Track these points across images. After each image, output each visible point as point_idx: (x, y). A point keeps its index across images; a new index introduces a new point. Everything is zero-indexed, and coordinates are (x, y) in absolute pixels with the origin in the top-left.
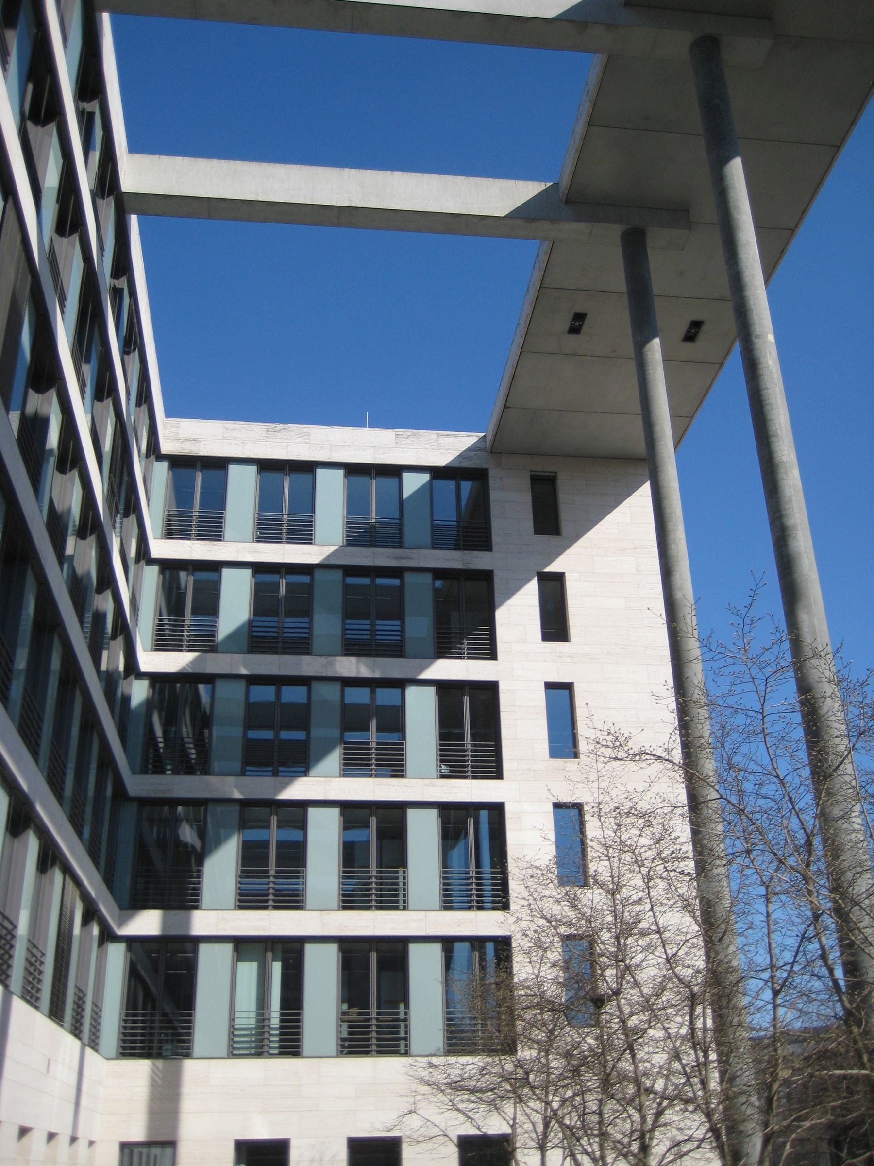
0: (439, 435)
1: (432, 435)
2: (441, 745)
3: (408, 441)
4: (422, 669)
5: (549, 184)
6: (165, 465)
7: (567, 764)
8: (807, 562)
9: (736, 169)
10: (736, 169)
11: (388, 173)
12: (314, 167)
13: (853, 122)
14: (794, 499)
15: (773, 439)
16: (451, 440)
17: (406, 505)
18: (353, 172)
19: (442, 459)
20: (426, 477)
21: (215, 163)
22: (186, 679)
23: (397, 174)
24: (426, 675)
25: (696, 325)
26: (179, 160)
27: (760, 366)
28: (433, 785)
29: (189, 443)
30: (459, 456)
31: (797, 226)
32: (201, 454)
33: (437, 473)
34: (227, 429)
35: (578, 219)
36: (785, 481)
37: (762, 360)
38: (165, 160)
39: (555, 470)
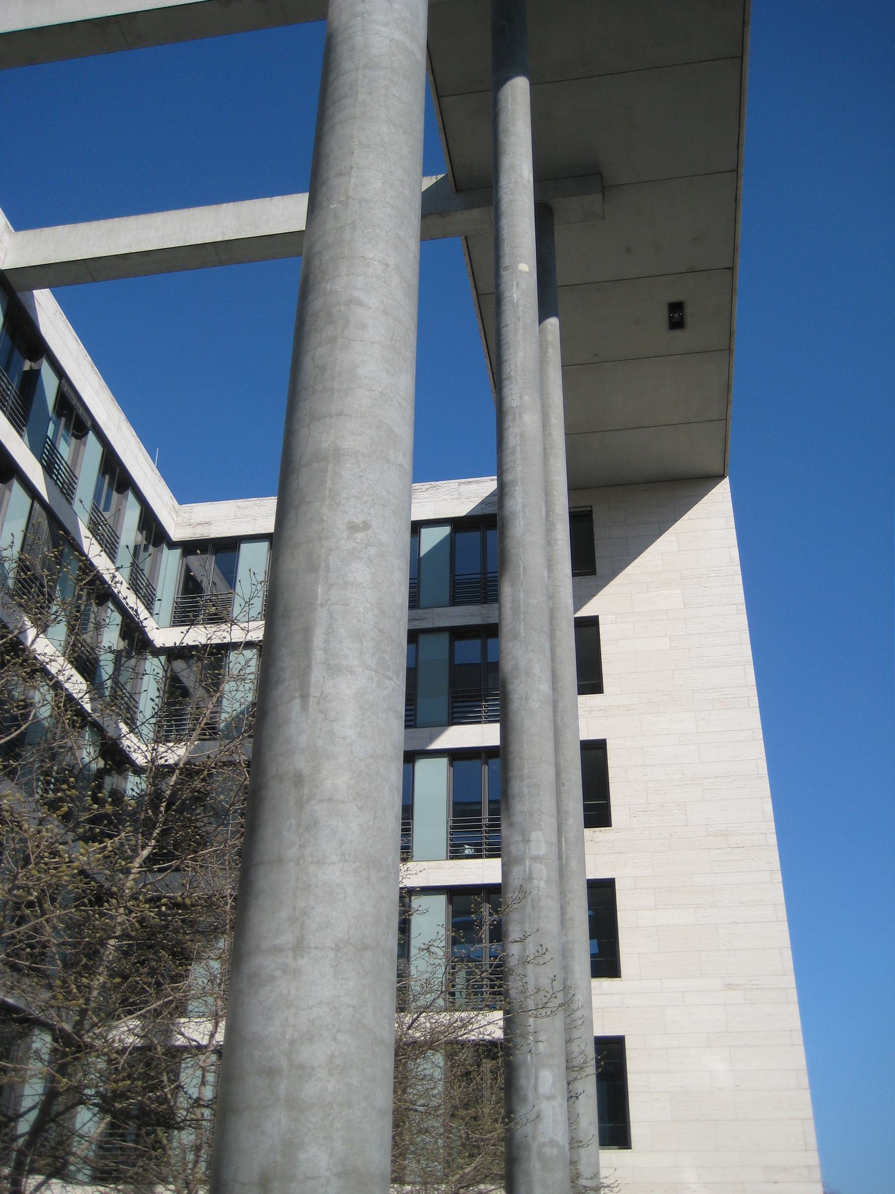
0: (460, 484)
1: (453, 484)
2: (454, 821)
3: (426, 494)
4: (432, 739)
5: (440, 177)
6: (178, 552)
7: (596, 835)
8: (522, 523)
9: (518, 93)
10: (518, 93)
11: (267, 199)
12: (191, 209)
13: (744, 23)
14: (518, 450)
15: (506, 383)
16: (473, 487)
17: (422, 562)
18: (231, 206)
19: (461, 509)
20: (446, 531)
21: (94, 224)
22: (189, 770)
23: (277, 200)
24: (437, 745)
25: (676, 307)
26: (60, 229)
27: (504, 301)
28: (440, 868)
29: (200, 526)
30: (481, 503)
31: (737, 167)
32: (212, 536)
33: (458, 524)
34: (239, 507)
35: (470, 206)
36: (511, 430)
37: (507, 294)
38: (47, 231)
39: (589, 504)
